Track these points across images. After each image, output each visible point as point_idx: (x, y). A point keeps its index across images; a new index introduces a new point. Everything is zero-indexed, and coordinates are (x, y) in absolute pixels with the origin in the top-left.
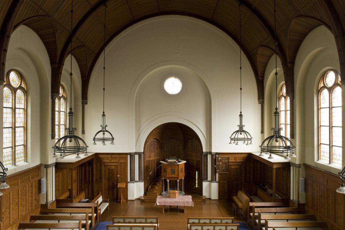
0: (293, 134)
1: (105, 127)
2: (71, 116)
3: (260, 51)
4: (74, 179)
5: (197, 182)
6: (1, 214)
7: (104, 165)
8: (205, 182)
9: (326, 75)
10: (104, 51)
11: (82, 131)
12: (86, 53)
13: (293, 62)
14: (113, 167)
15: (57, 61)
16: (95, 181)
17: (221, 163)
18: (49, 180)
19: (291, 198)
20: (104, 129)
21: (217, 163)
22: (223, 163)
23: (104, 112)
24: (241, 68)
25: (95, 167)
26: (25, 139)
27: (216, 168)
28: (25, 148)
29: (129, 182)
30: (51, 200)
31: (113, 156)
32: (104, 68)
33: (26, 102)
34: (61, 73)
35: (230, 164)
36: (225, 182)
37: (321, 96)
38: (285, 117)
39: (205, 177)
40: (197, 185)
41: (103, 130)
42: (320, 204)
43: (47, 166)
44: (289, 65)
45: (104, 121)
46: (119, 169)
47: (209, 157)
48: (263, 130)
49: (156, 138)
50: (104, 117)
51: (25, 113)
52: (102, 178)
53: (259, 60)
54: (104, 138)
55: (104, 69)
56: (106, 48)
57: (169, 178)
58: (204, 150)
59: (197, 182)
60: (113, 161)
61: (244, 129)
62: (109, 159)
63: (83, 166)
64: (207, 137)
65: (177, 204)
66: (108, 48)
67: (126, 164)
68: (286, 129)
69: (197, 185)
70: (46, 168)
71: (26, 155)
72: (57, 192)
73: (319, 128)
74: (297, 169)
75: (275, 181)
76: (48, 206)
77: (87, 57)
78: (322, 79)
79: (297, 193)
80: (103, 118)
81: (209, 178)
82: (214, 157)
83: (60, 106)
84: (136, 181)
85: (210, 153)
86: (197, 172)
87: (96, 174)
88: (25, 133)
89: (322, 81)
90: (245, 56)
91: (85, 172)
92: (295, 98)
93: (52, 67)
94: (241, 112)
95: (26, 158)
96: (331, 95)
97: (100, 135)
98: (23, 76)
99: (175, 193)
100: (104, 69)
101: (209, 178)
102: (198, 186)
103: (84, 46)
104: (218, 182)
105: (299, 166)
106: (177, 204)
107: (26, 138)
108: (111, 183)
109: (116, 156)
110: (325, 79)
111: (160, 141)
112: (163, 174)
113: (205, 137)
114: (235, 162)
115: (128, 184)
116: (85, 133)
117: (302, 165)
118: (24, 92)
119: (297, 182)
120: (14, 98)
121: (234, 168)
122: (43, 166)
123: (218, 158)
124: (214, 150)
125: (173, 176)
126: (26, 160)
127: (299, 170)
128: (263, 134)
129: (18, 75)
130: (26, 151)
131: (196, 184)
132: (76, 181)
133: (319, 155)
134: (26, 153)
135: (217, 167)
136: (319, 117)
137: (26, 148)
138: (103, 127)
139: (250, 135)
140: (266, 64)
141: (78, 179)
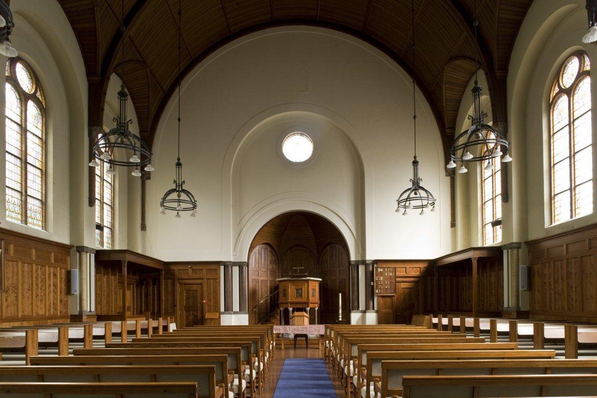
0: (507, 193)
1: (180, 183)
2: (123, 100)
3: (448, 69)
4: (127, 304)
5: (340, 311)
6: (1, 266)
7: (180, 284)
8: (356, 313)
9: (562, 69)
10: (178, 89)
11: (142, 224)
12: (148, 82)
13: (505, 68)
14: (194, 287)
15: (99, 68)
16: (163, 312)
17: (382, 278)
18: (84, 273)
19: (506, 305)
20: (179, 188)
21: (376, 278)
22: (386, 278)
23: (179, 159)
24: (415, 117)
25: (163, 287)
26: (44, 192)
27: (373, 286)
28: (44, 206)
29: (223, 313)
30: (89, 310)
31: (194, 267)
32: (179, 120)
33: (44, 127)
34: (103, 110)
35: (398, 279)
36: (390, 311)
37: (555, 112)
38: (493, 215)
39: (356, 305)
40: (340, 317)
41: (178, 189)
42: (556, 295)
43: (81, 249)
44: (498, 73)
45: (179, 174)
46: (205, 288)
47: (362, 269)
48: (455, 221)
49: (269, 242)
50: (179, 168)
51: (44, 146)
52: (176, 306)
53: (447, 94)
54: (178, 202)
55: (179, 121)
56: (183, 83)
57: (292, 303)
58: (353, 258)
59: (340, 311)
60: (194, 276)
61: (421, 184)
62: (188, 272)
63: (143, 285)
64: (357, 234)
65: (307, 331)
66: (187, 83)
67: (217, 279)
68: (494, 205)
69: (340, 317)
70: (79, 252)
71: (45, 220)
72: (99, 306)
73: (552, 168)
74: (515, 251)
75: (476, 280)
76: (83, 317)
77: (149, 91)
78: (555, 81)
79: (515, 294)
80: (178, 169)
81: (362, 306)
82: (371, 268)
83: (103, 169)
84: (236, 313)
85: (364, 262)
86: (340, 294)
87: (165, 300)
88: (44, 181)
89: (557, 86)
90: (421, 93)
91: (147, 295)
92: (509, 130)
93: (88, 81)
94: (415, 157)
95: (45, 224)
96: (571, 99)
97: (174, 196)
98: (40, 82)
99: (303, 316)
100: (179, 121)
101: (362, 306)
102: (342, 318)
103: (145, 62)
104: (377, 312)
105: (518, 246)
106: (307, 331)
107: (45, 190)
108: (191, 314)
109: (200, 267)
110: (560, 78)
111: (276, 249)
112: (281, 299)
113: (354, 236)
114: (406, 275)
115: (222, 316)
116: (146, 229)
117: (523, 245)
118: (41, 110)
119: (515, 274)
120: (23, 109)
121: (405, 288)
122: (75, 249)
123: (377, 270)
124: (370, 256)
125: (299, 300)
126: (45, 227)
127: (518, 252)
128: (454, 228)
129: (30, 75)
130: (45, 212)
131: (339, 315)
132: (132, 308)
133: (553, 216)
134: (45, 214)
135: (375, 286)
136: (552, 149)
137: (45, 207)
138: (178, 183)
139: (193, 197)
140: (459, 102)
141: (135, 307)
